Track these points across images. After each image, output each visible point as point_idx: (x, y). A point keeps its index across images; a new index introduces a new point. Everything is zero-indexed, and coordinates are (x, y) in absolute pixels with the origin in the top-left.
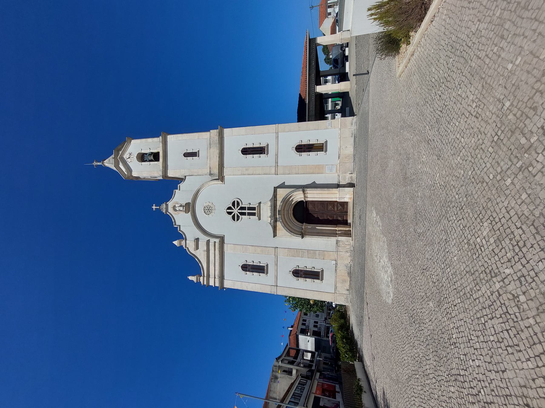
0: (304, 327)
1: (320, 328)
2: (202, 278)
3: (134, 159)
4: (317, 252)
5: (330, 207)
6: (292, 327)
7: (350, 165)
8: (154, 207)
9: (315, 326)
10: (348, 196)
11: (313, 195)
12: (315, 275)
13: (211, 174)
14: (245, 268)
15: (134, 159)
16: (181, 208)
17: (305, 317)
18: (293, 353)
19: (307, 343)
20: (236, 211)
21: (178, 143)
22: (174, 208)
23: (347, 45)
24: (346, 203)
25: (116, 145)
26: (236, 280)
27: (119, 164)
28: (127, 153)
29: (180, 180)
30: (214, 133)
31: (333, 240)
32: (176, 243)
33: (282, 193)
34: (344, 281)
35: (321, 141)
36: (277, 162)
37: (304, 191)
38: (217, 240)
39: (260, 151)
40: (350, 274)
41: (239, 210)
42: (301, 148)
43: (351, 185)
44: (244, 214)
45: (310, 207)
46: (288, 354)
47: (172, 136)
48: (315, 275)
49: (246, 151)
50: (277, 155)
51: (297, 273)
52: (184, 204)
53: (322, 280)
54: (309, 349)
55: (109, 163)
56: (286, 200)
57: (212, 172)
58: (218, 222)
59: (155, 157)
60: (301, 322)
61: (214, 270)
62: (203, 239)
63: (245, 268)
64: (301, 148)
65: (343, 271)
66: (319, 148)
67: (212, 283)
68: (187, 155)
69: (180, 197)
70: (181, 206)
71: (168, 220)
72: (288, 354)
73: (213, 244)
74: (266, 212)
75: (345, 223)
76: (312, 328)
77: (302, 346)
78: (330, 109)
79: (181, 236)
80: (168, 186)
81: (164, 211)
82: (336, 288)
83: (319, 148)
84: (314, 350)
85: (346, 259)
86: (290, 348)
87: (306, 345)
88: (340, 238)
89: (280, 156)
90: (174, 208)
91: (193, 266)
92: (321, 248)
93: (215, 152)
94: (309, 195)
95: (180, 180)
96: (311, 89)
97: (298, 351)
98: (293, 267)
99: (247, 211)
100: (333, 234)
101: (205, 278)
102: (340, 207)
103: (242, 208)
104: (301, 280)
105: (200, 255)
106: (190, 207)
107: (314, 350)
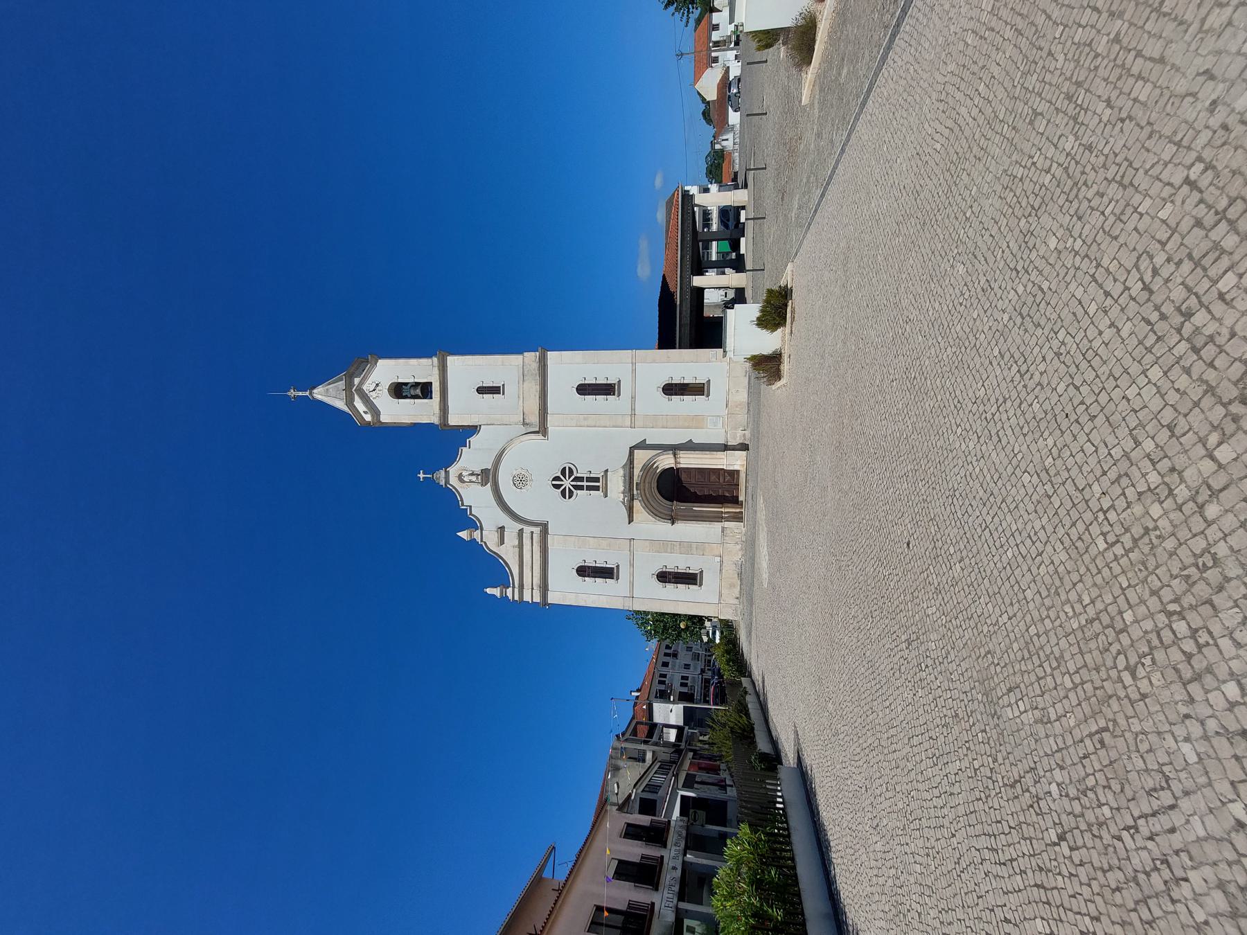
0: (662, 687)
1: (692, 687)
2: (509, 591)
3: (379, 391)
4: (694, 546)
5: (713, 478)
6: (638, 690)
7: (742, 417)
8: (421, 476)
9: (683, 685)
10: (739, 462)
11: (689, 460)
12: (689, 579)
13: (524, 424)
14: (583, 571)
15: (379, 391)
16: (474, 478)
17: (664, 670)
18: (643, 730)
19: (669, 714)
20: (567, 483)
21: (466, 371)
22: (460, 477)
23: (743, 208)
24: (738, 471)
25: (350, 362)
26: (568, 590)
27: (352, 400)
28: (369, 381)
29: (473, 430)
30: (531, 357)
31: (717, 527)
32: (464, 535)
33: (641, 457)
34: (732, 586)
35: (701, 380)
36: (633, 409)
37: (675, 455)
38: (537, 530)
39: (607, 389)
40: (740, 575)
41: (571, 482)
42: (672, 389)
43: (744, 447)
44: (581, 488)
45: (684, 477)
46: (635, 733)
47: (456, 358)
48: (689, 579)
49: (584, 389)
50: (633, 398)
51: (664, 577)
52: (478, 471)
53: (701, 585)
54: (673, 722)
55: (329, 394)
56: (648, 468)
57: (527, 421)
58: (536, 501)
59: (425, 390)
60: (657, 679)
61: (531, 577)
62: (512, 527)
63: (583, 571)
64: (672, 389)
65: (731, 571)
66: (698, 389)
67: (527, 598)
68: (482, 390)
69: (472, 458)
70: (472, 474)
71: (449, 497)
72: (635, 733)
73: (515, 534)
74: (616, 484)
75: (735, 501)
76: (678, 688)
77: (658, 718)
78: (714, 258)
79: (473, 524)
80: (448, 440)
81: (442, 483)
82: (720, 595)
83: (698, 389)
84: (681, 723)
85: (735, 554)
86: (638, 723)
87: (668, 717)
88: (727, 524)
89: (642, 399)
90: (460, 477)
91: (496, 571)
92: (698, 539)
93: (533, 388)
94: (682, 461)
95: (473, 430)
96: (685, 281)
97: (653, 727)
98: (658, 568)
99: (585, 484)
100: (718, 518)
101: (516, 590)
102: (728, 478)
103: (577, 479)
104: (670, 586)
105: (508, 553)
106: (488, 476)
107: (681, 723)
